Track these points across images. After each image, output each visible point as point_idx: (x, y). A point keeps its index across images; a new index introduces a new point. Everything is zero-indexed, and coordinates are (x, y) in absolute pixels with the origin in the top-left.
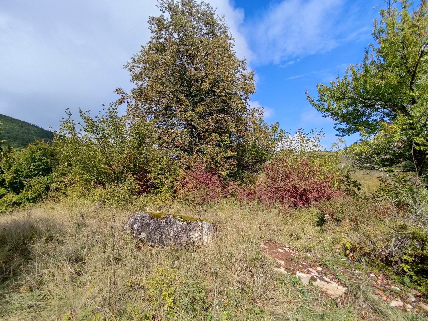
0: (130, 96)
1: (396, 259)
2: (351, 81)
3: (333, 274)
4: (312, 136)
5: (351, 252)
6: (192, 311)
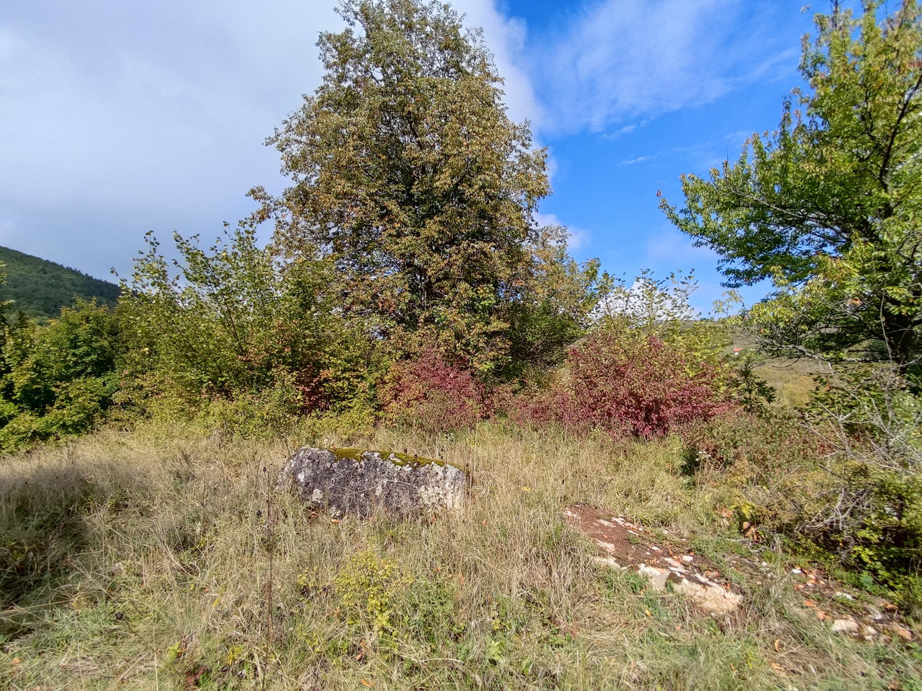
0: (282, 204)
1: (846, 536)
2: (753, 168)
3: (715, 569)
4: (671, 288)
5: (752, 524)
6: (427, 639)
